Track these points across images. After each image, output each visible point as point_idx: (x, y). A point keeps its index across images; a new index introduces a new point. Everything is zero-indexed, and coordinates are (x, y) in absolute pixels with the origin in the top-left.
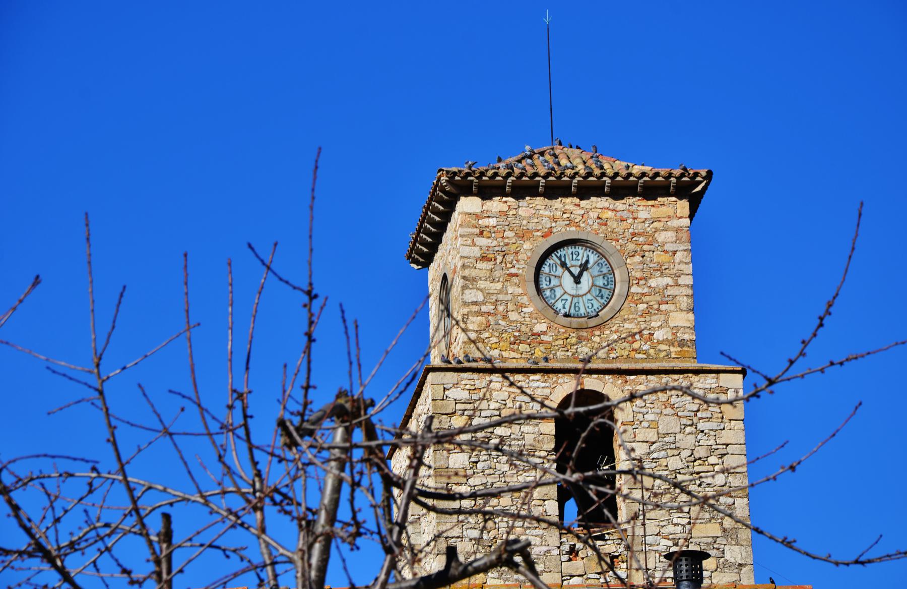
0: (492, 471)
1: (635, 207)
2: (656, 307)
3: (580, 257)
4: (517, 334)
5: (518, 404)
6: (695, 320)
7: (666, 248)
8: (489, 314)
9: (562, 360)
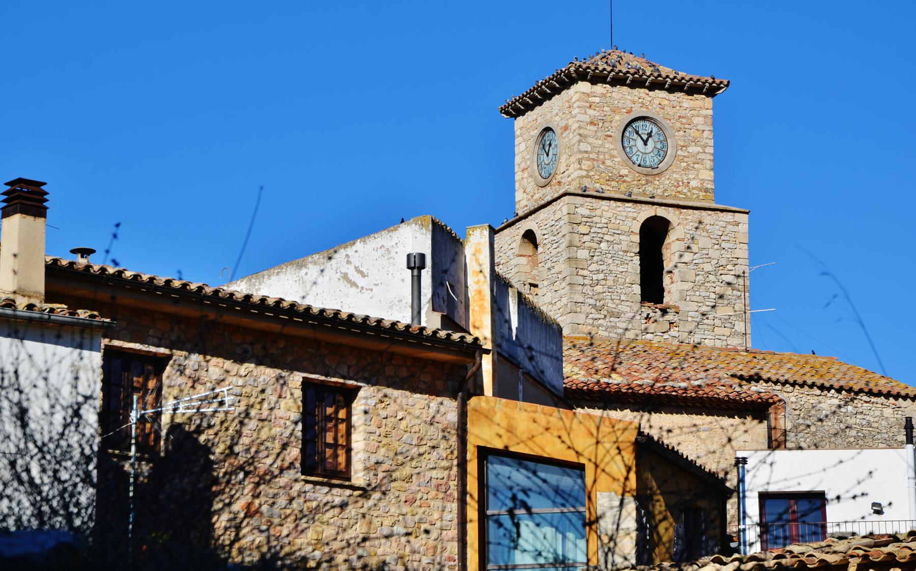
0: (602, 263)
1: (681, 99)
2: (692, 165)
3: (647, 129)
4: (611, 175)
5: (618, 221)
6: (714, 176)
7: (698, 128)
8: (594, 160)
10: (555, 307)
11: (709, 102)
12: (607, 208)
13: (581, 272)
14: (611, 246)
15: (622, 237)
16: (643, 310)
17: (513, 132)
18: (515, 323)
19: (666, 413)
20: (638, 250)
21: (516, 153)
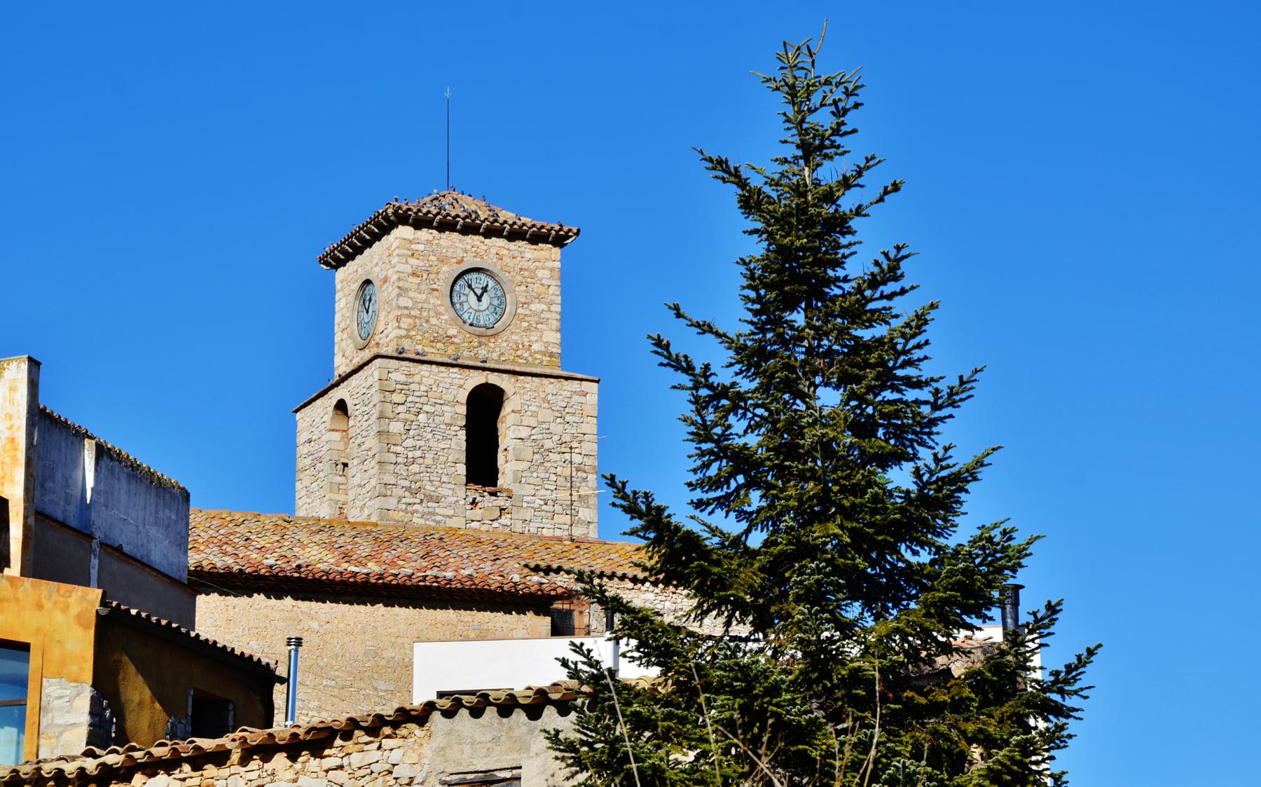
0: (420, 438)
1: (522, 249)
2: (534, 325)
4: (436, 335)
5: (440, 389)
8: (416, 317)
9: (468, 358)
10: (364, 491)
11: (556, 252)
12: (427, 374)
13: (393, 449)
14: (432, 419)
15: (444, 408)
16: (468, 493)
17: (334, 286)
18: (90, 483)
19: (428, 608)
20: (464, 423)
21: (336, 310)
